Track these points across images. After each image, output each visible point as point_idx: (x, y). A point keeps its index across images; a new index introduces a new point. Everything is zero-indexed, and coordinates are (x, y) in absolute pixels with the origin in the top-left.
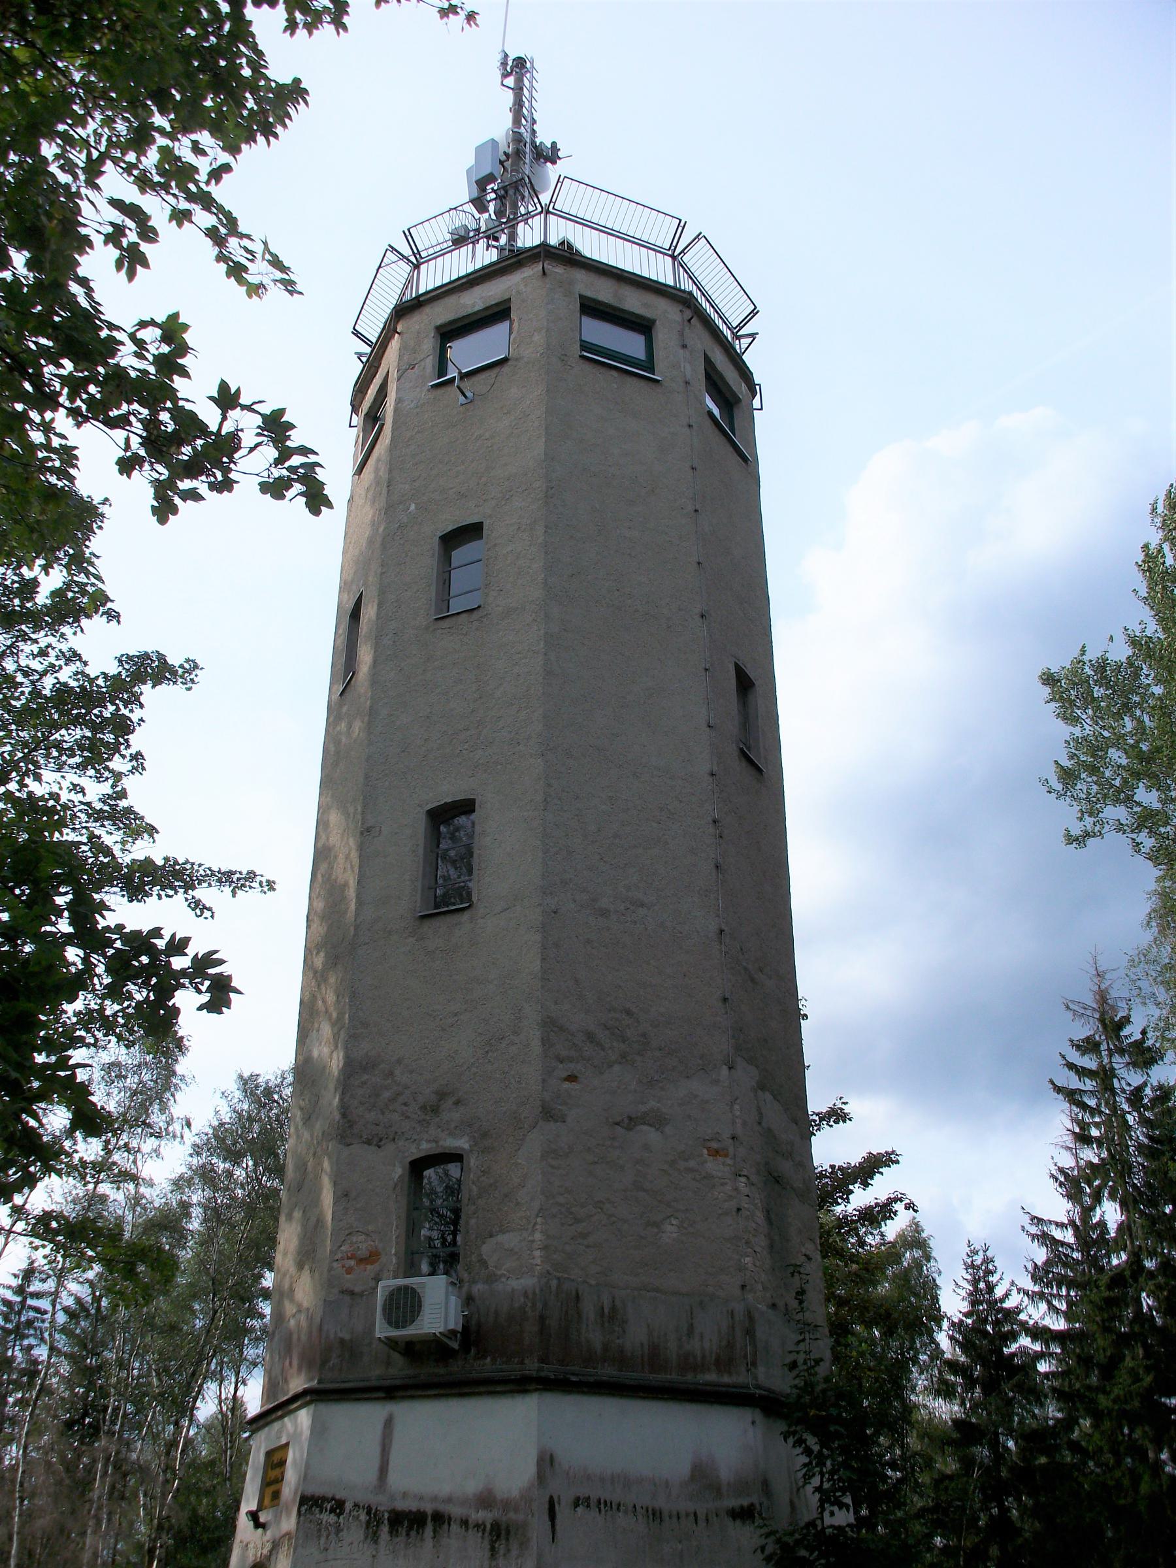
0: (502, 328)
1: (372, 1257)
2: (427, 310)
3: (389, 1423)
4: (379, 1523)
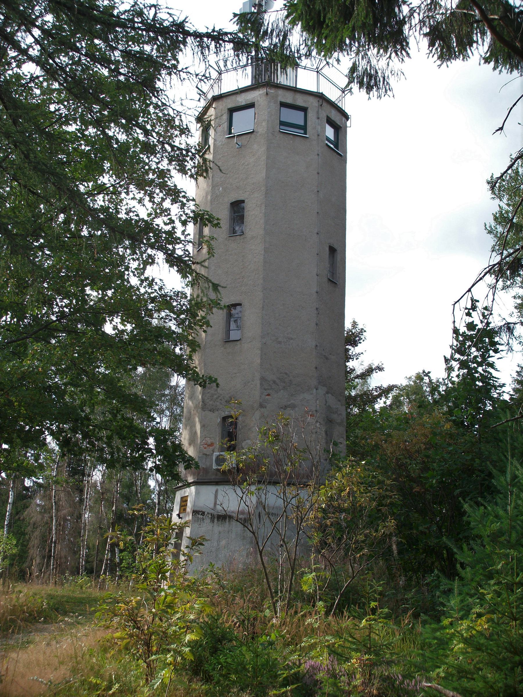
0: (251, 111)
1: (212, 444)
2: (225, 100)
3: (217, 491)
4: (214, 518)
